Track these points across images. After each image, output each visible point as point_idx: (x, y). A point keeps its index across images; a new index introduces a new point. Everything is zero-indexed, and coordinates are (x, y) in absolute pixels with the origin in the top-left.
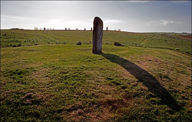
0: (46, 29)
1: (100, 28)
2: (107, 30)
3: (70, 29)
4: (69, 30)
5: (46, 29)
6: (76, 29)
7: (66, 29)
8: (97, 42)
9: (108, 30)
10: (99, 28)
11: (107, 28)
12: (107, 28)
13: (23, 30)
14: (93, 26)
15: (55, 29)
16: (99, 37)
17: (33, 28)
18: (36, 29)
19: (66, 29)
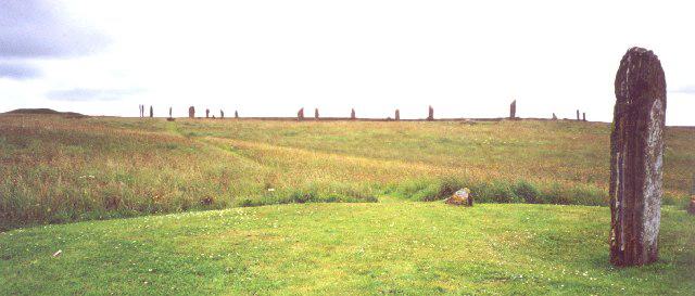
0: (196, 115)
1: (657, 112)
2: (513, 117)
3: (321, 116)
4: (317, 118)
5: (200, 113)
6: (349, 116)
7: (301, 112)
8: (641, 198)
9: (518, 119)
10: (652, 114)
11: (513, 107)
12: (513, 107)
13: (78, 116)
14: (613, 100)
15: (240, 115)
16: (653, 169)
17: (126, 109)
18: (581, 118)
19: (301, 112)
